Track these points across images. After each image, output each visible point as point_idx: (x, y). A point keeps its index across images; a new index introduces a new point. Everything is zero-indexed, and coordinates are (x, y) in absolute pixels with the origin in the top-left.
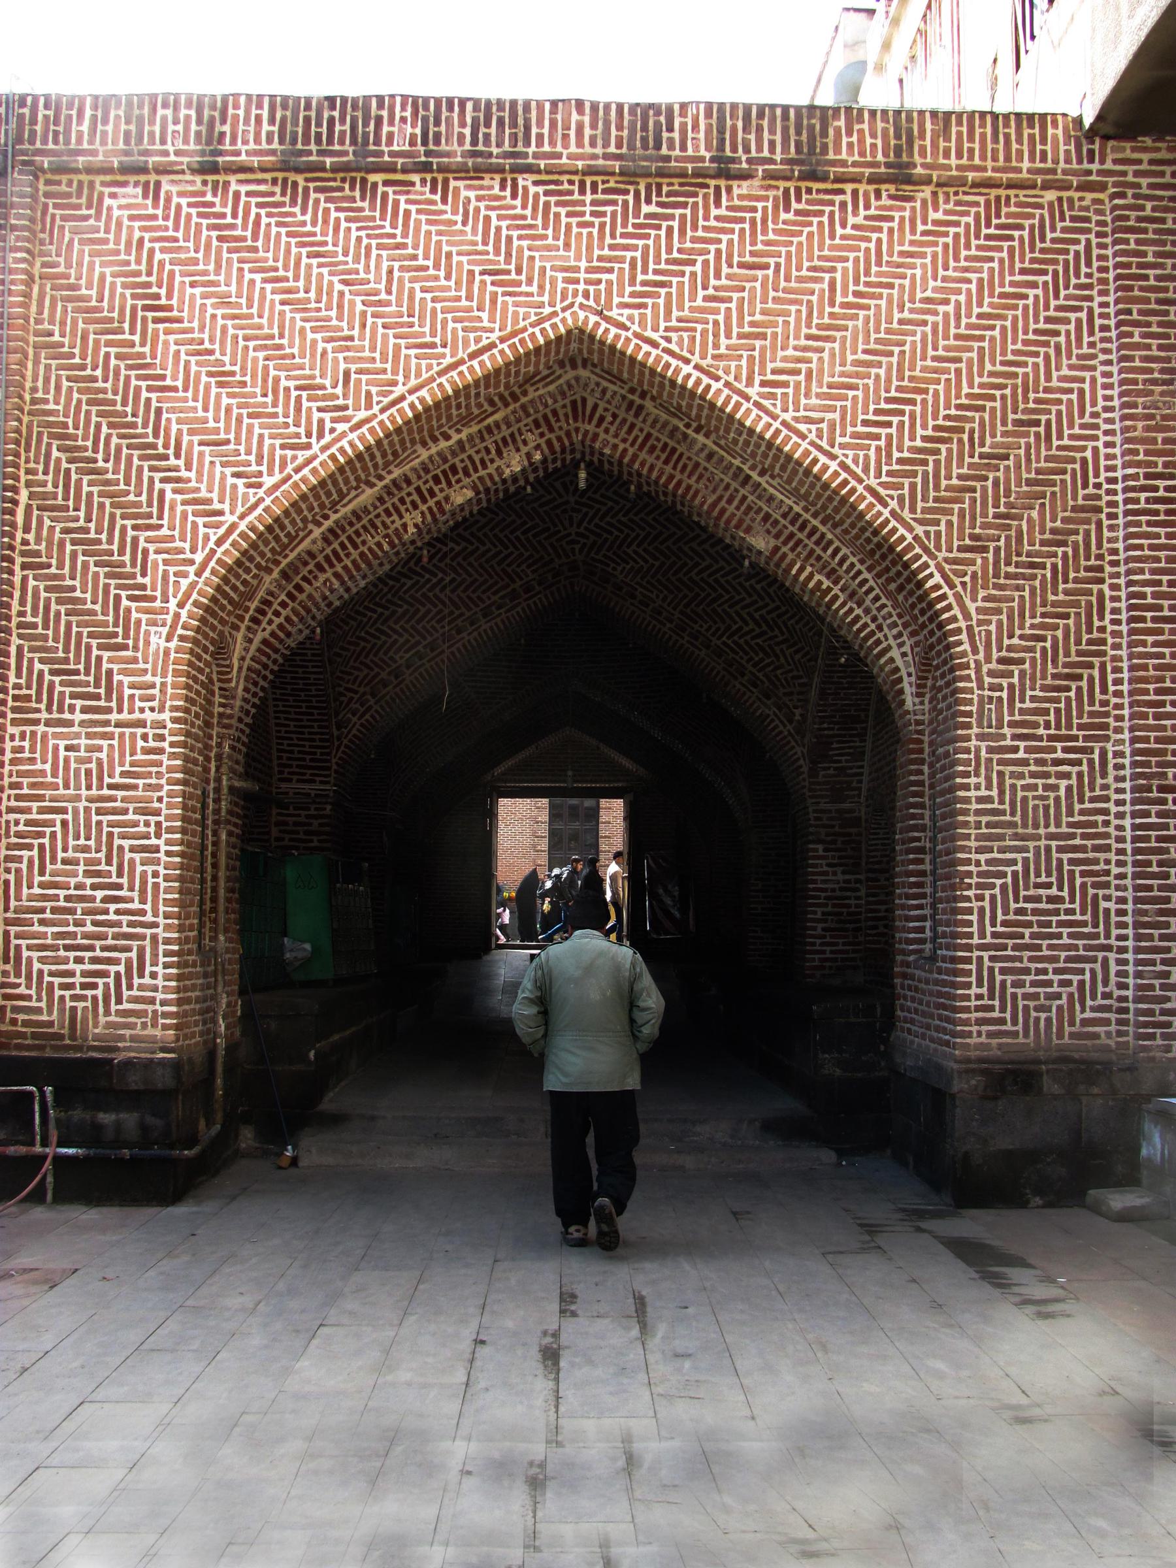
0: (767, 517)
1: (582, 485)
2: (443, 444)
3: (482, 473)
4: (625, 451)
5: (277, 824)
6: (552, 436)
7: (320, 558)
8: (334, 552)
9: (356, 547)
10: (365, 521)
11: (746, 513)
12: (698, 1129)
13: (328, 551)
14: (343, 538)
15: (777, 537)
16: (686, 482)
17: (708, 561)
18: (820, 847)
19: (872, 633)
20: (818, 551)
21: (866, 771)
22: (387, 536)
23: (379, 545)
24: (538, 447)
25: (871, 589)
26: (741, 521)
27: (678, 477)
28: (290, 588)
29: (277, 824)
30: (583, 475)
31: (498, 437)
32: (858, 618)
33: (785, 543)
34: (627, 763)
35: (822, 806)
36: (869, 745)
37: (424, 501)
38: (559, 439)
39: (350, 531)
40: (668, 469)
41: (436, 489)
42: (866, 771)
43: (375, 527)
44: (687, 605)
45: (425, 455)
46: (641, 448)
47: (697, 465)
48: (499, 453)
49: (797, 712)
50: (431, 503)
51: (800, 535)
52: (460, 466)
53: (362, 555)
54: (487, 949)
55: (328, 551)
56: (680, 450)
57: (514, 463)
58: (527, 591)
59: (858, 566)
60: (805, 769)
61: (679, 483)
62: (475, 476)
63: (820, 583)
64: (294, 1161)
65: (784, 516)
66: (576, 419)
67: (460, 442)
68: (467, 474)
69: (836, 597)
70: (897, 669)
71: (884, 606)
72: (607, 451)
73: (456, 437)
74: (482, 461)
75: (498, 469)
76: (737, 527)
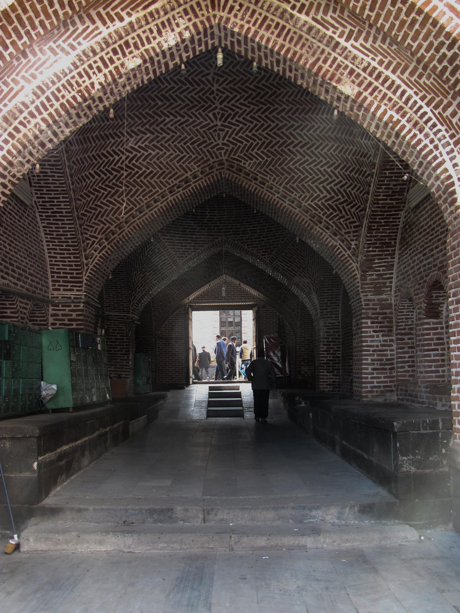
0: (352, 72)
1: (220, 62)
2: (118, 25)
3: (147, 46)
4: (249, 29)
5: (52, 315)
6: (197, 21)
7: (32, 108)
8: (43, 104)
9: (57, 99)
10: (64, 81)
11: (337, 69)
12: (314, 513)
13: (38, 102)
14: (48, 93)
15: (359, 85)
16: (293, 49)
17: (299, 157)
18: (369, 321)
19: (431, 152)
20: (390, 94)
21: (394, 276)
22: (80, 91)
23: (74, 98)
24: (187, 28)
25: (430, 119)
26: (333, 75)
27: (287, 45)
28: (10, 129)
29: (52, 315)
30: (220, 56)
31: (159, 22)
32: (420, 141)
33: (366, 89)
34: (254, 292)
35: (369, 297)
36: (396, 260)
37: (106, 66)
38: (202, 22)
39: (54, 89)
40: (280, 41)
41: (115, 58)
42: (394, 276)
43: (72, 86)
44: (287, 183)
45: (105, 32)
46: (260, 27)
47: (301, 37)
48: (160, 33)
49: (353, 243)
50: (111, 68)
51: (376, 84)
52: (131, 42)
53: (62, 105)
54: (188, 384)
55: (38, 102)
56: (288, 27)
57: (170, 39)
58: (195, 177)
59: (420, 103)
60: (359, 276)
61: (288, 50)
62: (142, 49)
63: (392, 117)
64: (17, 547)
65: (364, 70)
66: (213, 9)
67: (131, 24)
68: (137, 48)
69: (404, 127)
70: (450, 177)
71: (440, 131)
72: (236, 30)
73: (127, 20)
74: (147, 38)
75: (158, 44)
76: (331, 79)
